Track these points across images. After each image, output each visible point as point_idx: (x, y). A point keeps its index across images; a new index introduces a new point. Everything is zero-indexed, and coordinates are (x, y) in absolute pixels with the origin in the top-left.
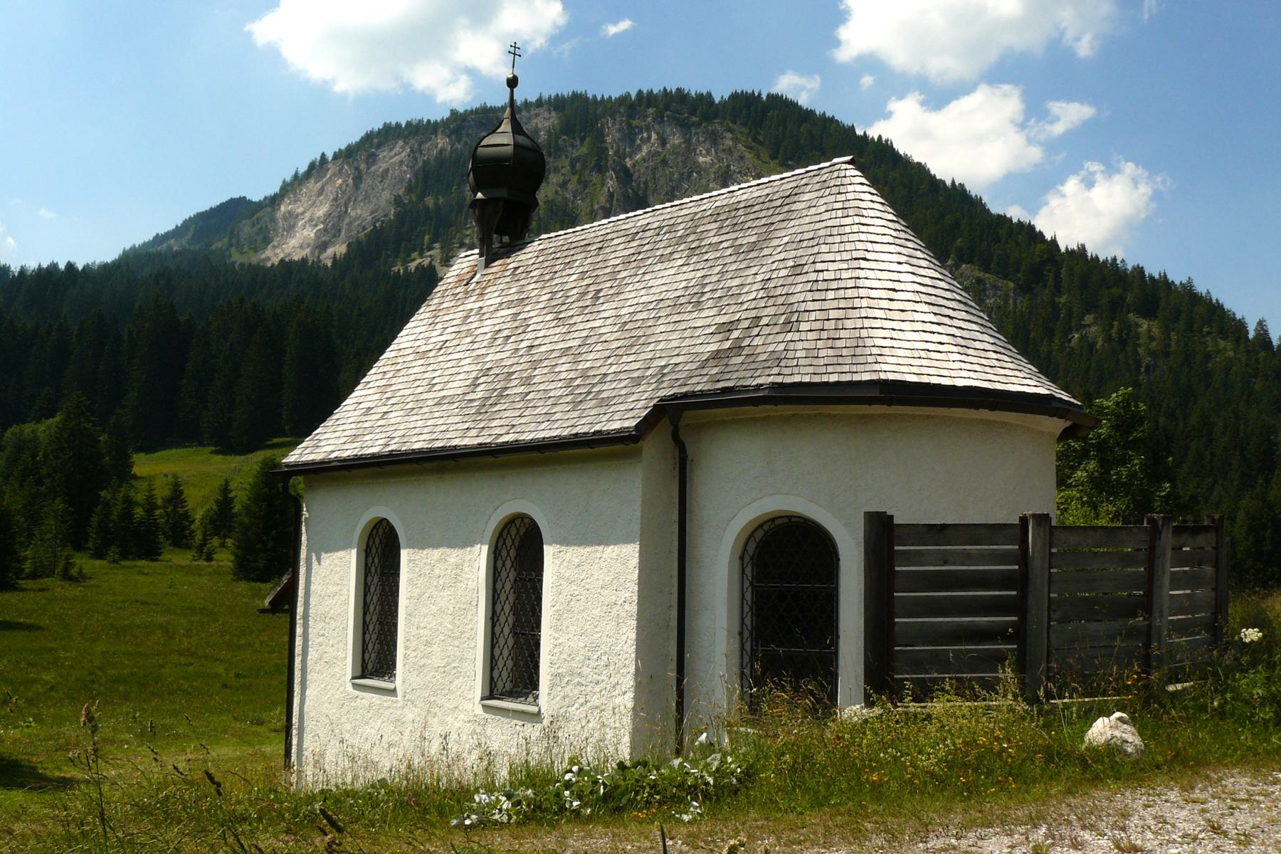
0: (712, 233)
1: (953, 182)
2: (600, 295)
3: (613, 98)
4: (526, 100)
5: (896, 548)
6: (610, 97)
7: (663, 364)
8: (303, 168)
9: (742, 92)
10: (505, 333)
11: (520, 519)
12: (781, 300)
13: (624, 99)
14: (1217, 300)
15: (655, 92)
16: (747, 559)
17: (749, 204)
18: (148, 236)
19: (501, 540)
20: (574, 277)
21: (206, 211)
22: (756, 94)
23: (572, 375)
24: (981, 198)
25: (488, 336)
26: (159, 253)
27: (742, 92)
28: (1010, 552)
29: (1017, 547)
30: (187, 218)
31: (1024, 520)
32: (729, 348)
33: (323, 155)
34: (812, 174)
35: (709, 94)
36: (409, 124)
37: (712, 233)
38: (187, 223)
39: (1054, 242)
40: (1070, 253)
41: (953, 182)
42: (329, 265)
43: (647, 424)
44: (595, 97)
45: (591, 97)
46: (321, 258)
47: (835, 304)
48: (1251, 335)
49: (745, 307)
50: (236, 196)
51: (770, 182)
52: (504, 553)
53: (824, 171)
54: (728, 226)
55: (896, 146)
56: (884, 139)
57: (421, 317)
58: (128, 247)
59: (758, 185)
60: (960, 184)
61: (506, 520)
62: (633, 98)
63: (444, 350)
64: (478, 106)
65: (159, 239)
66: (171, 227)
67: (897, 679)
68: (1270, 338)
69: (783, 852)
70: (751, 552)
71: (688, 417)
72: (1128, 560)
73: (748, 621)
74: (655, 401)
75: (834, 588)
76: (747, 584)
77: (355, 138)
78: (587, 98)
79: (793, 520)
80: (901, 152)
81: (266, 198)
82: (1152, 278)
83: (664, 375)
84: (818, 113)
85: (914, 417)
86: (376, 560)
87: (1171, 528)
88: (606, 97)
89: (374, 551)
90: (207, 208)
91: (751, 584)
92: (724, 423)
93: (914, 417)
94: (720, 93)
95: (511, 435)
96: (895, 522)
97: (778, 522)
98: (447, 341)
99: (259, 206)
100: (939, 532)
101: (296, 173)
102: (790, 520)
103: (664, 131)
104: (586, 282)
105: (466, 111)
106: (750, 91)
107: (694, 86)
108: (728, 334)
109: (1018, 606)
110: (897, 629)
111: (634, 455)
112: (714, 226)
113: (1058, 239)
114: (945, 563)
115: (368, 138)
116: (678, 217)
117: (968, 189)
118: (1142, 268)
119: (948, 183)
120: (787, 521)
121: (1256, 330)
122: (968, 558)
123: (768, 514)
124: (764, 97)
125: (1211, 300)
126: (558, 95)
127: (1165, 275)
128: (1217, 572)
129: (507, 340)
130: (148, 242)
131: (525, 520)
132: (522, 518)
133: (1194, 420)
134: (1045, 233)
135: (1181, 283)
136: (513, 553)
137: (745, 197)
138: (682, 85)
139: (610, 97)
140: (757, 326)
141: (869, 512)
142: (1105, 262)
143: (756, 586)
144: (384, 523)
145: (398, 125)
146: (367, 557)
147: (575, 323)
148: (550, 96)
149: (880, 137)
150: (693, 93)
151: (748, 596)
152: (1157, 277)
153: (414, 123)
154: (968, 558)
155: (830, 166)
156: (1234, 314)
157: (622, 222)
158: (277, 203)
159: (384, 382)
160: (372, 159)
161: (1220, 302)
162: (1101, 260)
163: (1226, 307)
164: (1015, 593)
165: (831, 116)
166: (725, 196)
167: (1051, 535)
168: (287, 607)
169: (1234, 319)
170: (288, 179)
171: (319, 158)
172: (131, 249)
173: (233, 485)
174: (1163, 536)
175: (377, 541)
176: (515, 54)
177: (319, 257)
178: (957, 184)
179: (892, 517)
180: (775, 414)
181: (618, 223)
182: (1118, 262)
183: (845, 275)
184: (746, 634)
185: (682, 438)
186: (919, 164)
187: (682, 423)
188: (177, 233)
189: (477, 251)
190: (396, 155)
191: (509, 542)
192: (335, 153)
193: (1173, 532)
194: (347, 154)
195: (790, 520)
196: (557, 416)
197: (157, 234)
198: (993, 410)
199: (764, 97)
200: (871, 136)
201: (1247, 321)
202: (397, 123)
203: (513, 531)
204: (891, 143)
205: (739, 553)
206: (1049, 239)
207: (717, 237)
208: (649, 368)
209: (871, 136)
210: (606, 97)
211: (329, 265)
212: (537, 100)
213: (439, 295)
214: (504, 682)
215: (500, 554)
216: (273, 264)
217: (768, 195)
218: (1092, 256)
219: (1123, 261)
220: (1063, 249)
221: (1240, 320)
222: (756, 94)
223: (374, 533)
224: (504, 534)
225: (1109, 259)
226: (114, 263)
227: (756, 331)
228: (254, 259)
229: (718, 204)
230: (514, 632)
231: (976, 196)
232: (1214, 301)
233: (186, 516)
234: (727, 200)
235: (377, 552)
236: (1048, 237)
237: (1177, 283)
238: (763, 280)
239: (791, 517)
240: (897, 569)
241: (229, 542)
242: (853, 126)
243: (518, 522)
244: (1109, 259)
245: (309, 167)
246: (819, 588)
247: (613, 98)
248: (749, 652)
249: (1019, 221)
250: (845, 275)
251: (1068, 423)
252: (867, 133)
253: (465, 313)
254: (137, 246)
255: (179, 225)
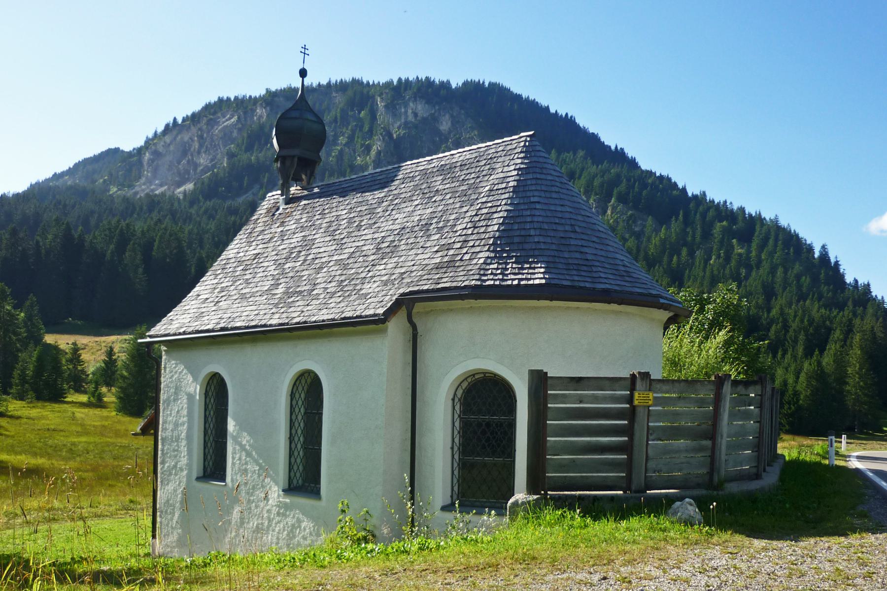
0: (438, 183)
1: (616, 147)
2: (363, 224)
3: (381, 83)
4: (319, 83)
5: (549, 392)
6: (379, 83)
7: (403, 271)
8: (160, 129)
9: (472, 80)
10: (298, 249)
11: (308, 374)
12: (482, 230)
13: (389, 84)
14: (795, 231)
15: (411, 79)
16: (456, 400)
17: (463, 163)
18: (49, 175)
19: (295, 387)
20: (345, 212)
21: (91, 157)
22: (481, 82)
23: (343, 278)
24: (635, 158)
25: (287, 250)
26: (57, 187)
27: (472, 80)
28: (622, 396)
29: (549, 392)
30: (77, 162)
31: (633, 376)
32: (447, 262)
33: (175, 119)
34: (506, 143)
35: (448, 82)
36: (236, 98)
37: (438, 183)
38: (77, 166)
39: (684, 190)
40: (695, 197)
41: (616, 147)
42: (181, 197)
43: (391, 312)
44: (368, 83)
45: (365, 82)
46: (175, 192)
47: (518, 233)
48: (817, 255)
49: (458, 234)
50: (113, 147)
51: (478, 148)
52: (297, 396)
53: (514, 142)
54: (449, 178)
55: (577, 121)
56: (569, 116)
57: (241, 237)
58: (34, 182)
59: (470, 150)
60: (621, 148)
61: (298, 374)
62: (395, 84)
63: (256, 260)
64: (286, 86)
65: (56, 176)
66: (66, 168)
67: (548, 476)
68: (829, 257)
69: (505, 590)
70: (459, 396)
71: (418, 307)
72: (701, 403)
73: (457, 440)
74: (396, 297)
75: (513, 419)
76: (456, 416)
77: (197, 107)
78: (362, 83)
79: (487, 375)
80: (581, 125)
81: (134, 149)
82: (750, 215)
83: (403, 279)
84: (524, 97)
85: (568, 308)
86: (212, 401)
87: (730, 381)
88: (376, 82)
89: (210, 394)
90: (92, 155)
91: (459, 416)
92: (443, 311)
93: (568, 308)
94: (456, 82)
95: (301, 318)
96: (548, 375)
97: (477, 377)
98: (259, 253)
99: (130, 154)
100: (577, 382)
101: (156, 132)
102: (485, 375)
103: (416, 107)
104: (352, 215)
105: (277, 90)
106: (477, 80)
107: (438, 77)
108: (446, 252)
109: (628, 431)
110: (548, 444)
111: (420, 329)
112: (441, 178)
113: (687, 188)
114: (581, 402)
115: (208, 107)
116: (416, 171)
117: (626, 152)
118: (744, 208)
119: (613, 148)
120: (483, 376)
121: (820, 252)
122: (596, 399)
123: (469, 371)
124: (487, 84)
125: (790, 231)
126: (342, 80)
127: (760, 214)
128: (761, 411)
129: (299, 254)
130: (49, 178)
131: (311, 374)
132: (309, 373)
133: (774, 312)
134: (678, 183)
135: (770, 219)
136: (303, 396)
137: (461, 158)
138: (429, 75)
139: (379, 83)
140: (466, 247)
141: (531, 370)
142: (719, 203)
143: (462, 418)
144: (217, 376)
145: (228, 99)
146: (206, 398)
147: (345, 243)
148: (336, 81)
149: (567, 114)
150: (437, 81)
151: (457, 424)
152: (754, 214)
153: (240, 97)
154: (596, 399)
155: (518, 138)
156: (805, 240)
157: (378, 174)
158: (142, 152)
159: (216, 281)
160: (212, 123)
161: (797, 233)
162: (716, 202)
163: (801, 235)
164: (626, 422)
165: (533, 99)
166: (447, 158)
167: (650, 385)
168: (152, 431)
169: (806, 244)
170: (150, 136)
171: (172, 121)
172: (36, 183)
173: (116, 350)
174: (725, 387)
175: (213, 388)
176: (305, 53)
177: (174, 192)
178: (619, 148)
179: (546, 373)
180: (477, 305)
181: (375, 175)
182: (728, 204)
183: (525, 213)
184: (456, 449)
185: (415, 320)
186: (593, 134)
187: (415, 311)
188: (70, 172)
189: (279, 192)
190: (227, 120)
191: (300, 389)
192: (183, 118)
193: (732, 384)
194: (194, 118)
195: (485, 375)
196: (333, 305)
197: (55, 173)
198: (620, 304)
199: (487, 84)
200: (560, 114)
201: (814, 245)
202: (227, 97)
203: (303, 381)
204: (574, 119)
205: (290, 393)
206: (681, 188)
207: (441, 186)
208: (394, 274)
209: (560, 114)
210: (376, 82)
211: (181, 197)
212: (327, 84)
213: (253, 222)
214: (298, 481)
215: (294, 396)
216: (141, 197)
217: (476, 157)
218: (710, 200)
219: (731, 203)
220: (690, 194)
221: (809, 245)
222: (481, 82)
223: (211, 382)
224: (297, 384)
225: (722, 202)
226: (24, 192)
227: (465, 250)
228: (129, 193)
229: (443, 163)
230: (305, 449)
231: (632, 157)
232: (793, 231)
233: (83, 371)
234: (449, 161)
235: (212, 395)
236: (680, 186)
237: (768, 219)
238: (471, 216)
239: (486, 373)
240: (549, 405)
241: (114, 389)
242: (548, 106)
243: (306, 375)
244: (722, 202)
245: (165, 127)
246: (481, 418)
247: (381, 83)
248: (457, 460)
249: (660, 174)
250: (525, 213)
251: (671, 314)
252: (558, 112)
253: (271, 235)
254: (41, 181)
255: (71, 167)
